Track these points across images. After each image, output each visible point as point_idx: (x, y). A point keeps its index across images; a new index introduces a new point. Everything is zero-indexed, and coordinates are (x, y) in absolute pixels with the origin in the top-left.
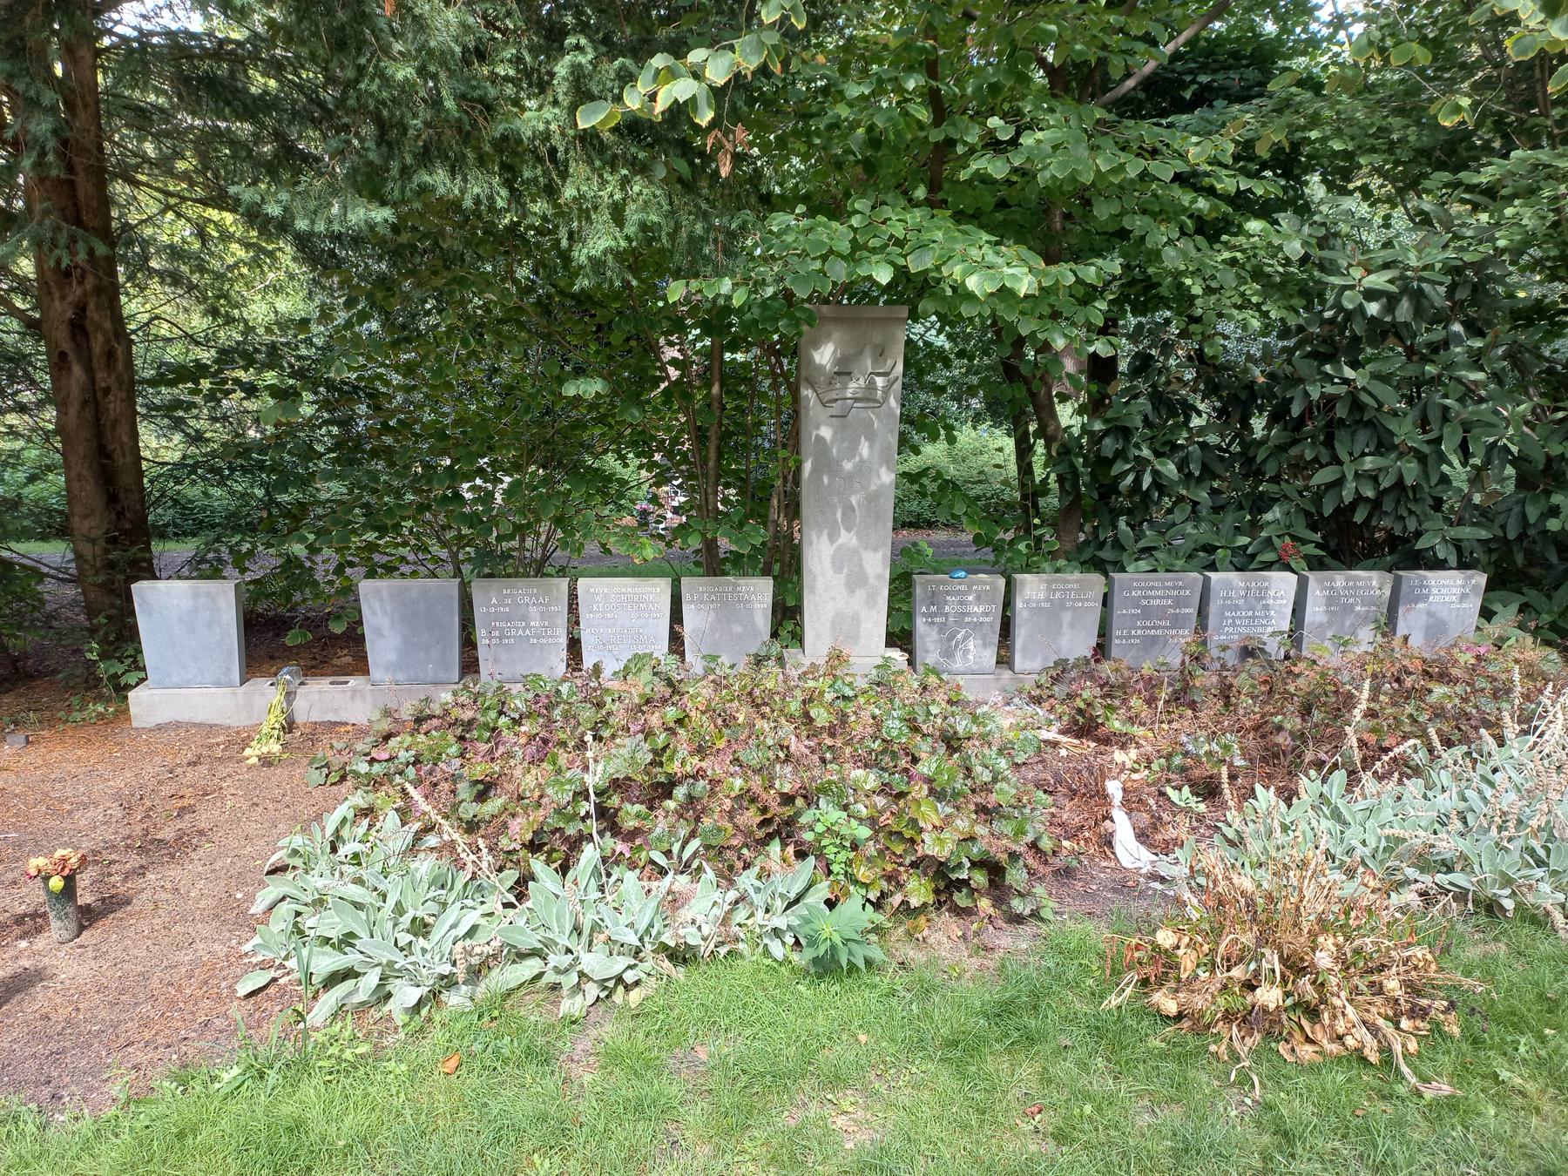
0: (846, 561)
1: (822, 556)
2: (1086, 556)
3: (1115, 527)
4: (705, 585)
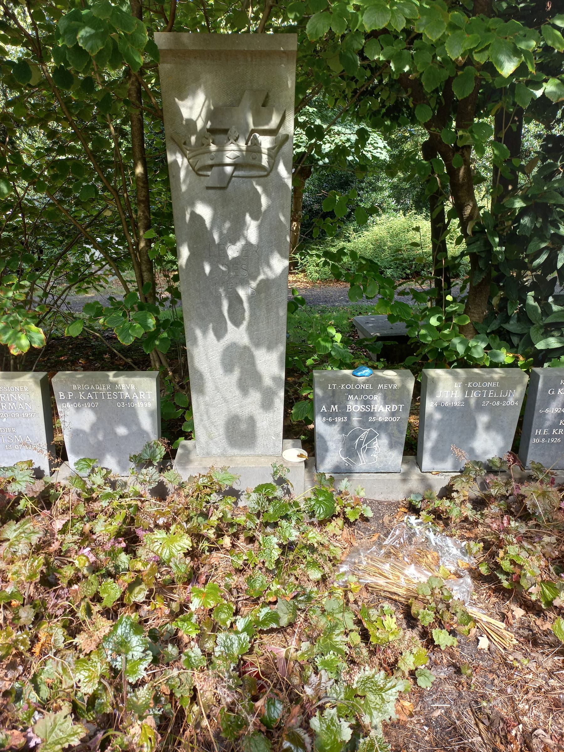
0: (239, 361)
1: (206, 352)
2: (494, 326)
3: (524, 300)
4: (80, 381)
